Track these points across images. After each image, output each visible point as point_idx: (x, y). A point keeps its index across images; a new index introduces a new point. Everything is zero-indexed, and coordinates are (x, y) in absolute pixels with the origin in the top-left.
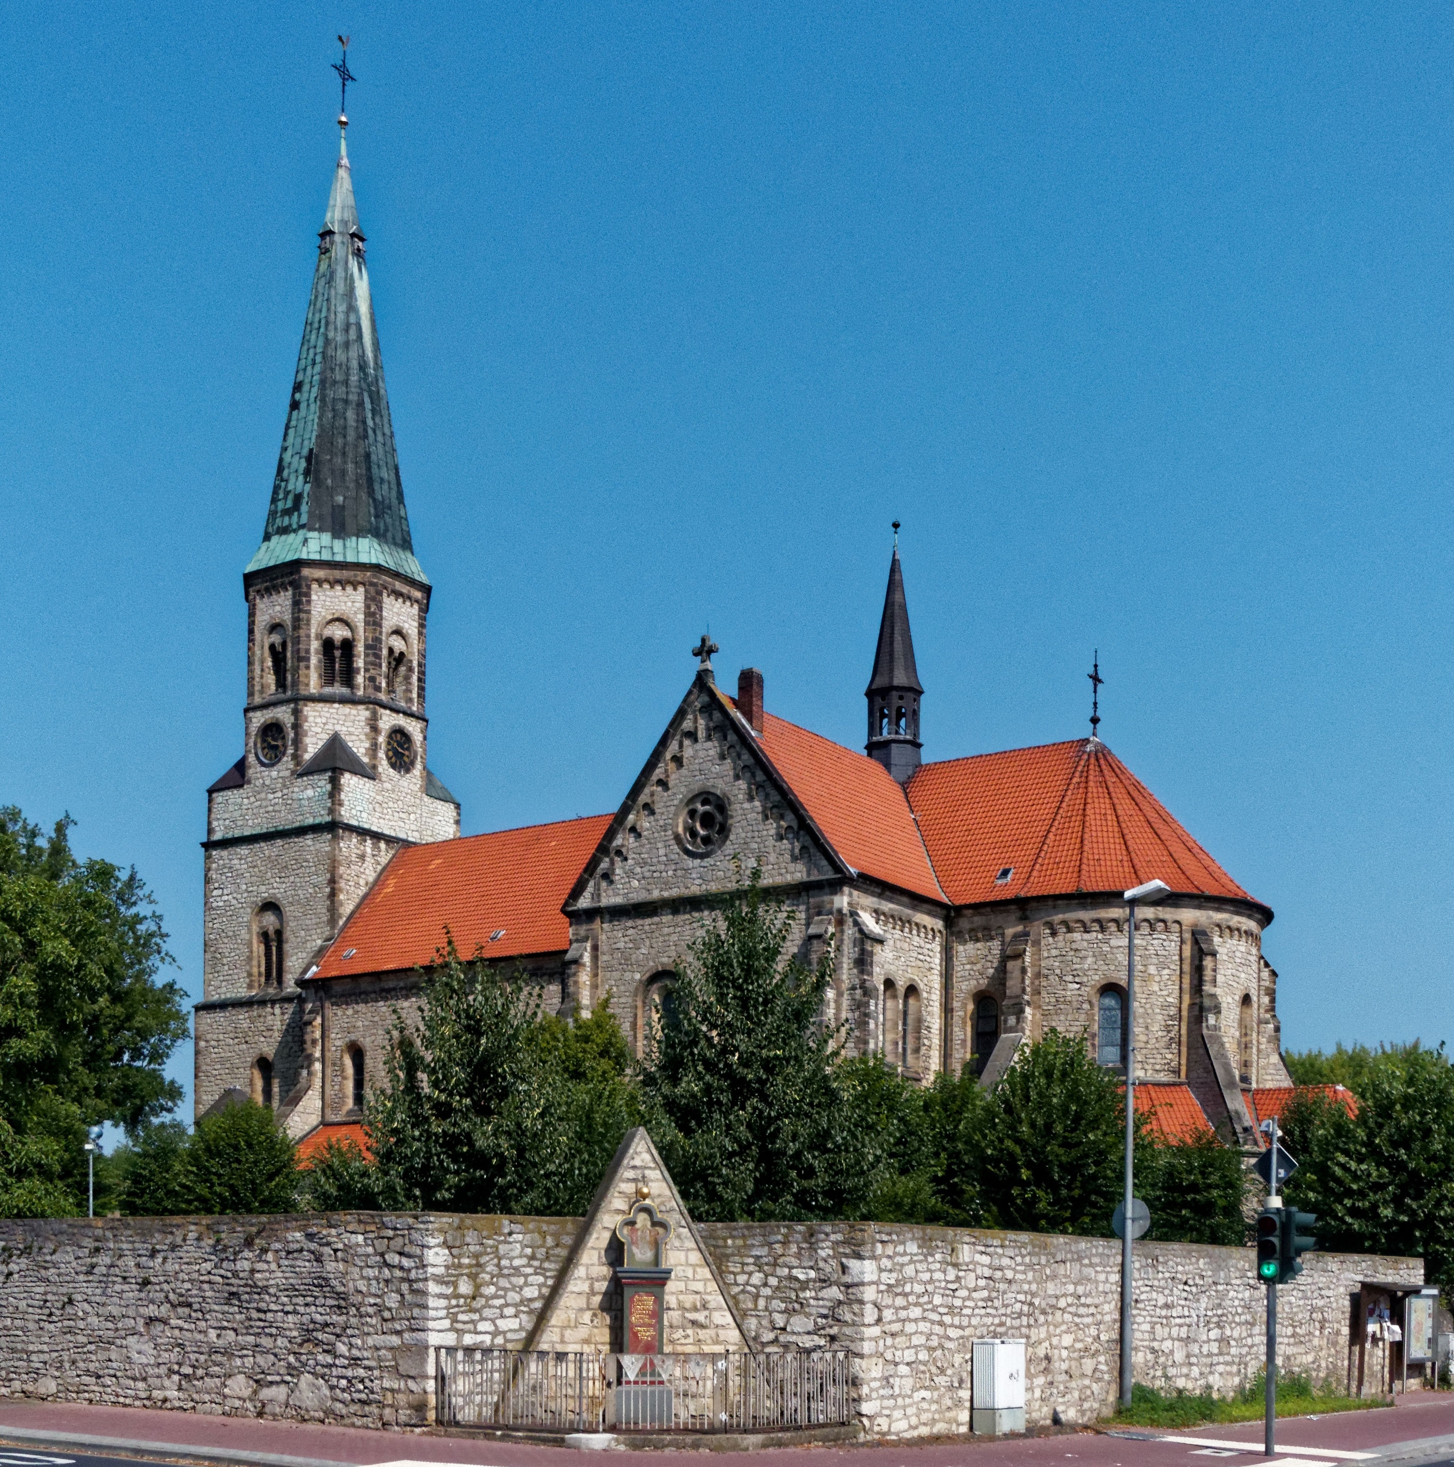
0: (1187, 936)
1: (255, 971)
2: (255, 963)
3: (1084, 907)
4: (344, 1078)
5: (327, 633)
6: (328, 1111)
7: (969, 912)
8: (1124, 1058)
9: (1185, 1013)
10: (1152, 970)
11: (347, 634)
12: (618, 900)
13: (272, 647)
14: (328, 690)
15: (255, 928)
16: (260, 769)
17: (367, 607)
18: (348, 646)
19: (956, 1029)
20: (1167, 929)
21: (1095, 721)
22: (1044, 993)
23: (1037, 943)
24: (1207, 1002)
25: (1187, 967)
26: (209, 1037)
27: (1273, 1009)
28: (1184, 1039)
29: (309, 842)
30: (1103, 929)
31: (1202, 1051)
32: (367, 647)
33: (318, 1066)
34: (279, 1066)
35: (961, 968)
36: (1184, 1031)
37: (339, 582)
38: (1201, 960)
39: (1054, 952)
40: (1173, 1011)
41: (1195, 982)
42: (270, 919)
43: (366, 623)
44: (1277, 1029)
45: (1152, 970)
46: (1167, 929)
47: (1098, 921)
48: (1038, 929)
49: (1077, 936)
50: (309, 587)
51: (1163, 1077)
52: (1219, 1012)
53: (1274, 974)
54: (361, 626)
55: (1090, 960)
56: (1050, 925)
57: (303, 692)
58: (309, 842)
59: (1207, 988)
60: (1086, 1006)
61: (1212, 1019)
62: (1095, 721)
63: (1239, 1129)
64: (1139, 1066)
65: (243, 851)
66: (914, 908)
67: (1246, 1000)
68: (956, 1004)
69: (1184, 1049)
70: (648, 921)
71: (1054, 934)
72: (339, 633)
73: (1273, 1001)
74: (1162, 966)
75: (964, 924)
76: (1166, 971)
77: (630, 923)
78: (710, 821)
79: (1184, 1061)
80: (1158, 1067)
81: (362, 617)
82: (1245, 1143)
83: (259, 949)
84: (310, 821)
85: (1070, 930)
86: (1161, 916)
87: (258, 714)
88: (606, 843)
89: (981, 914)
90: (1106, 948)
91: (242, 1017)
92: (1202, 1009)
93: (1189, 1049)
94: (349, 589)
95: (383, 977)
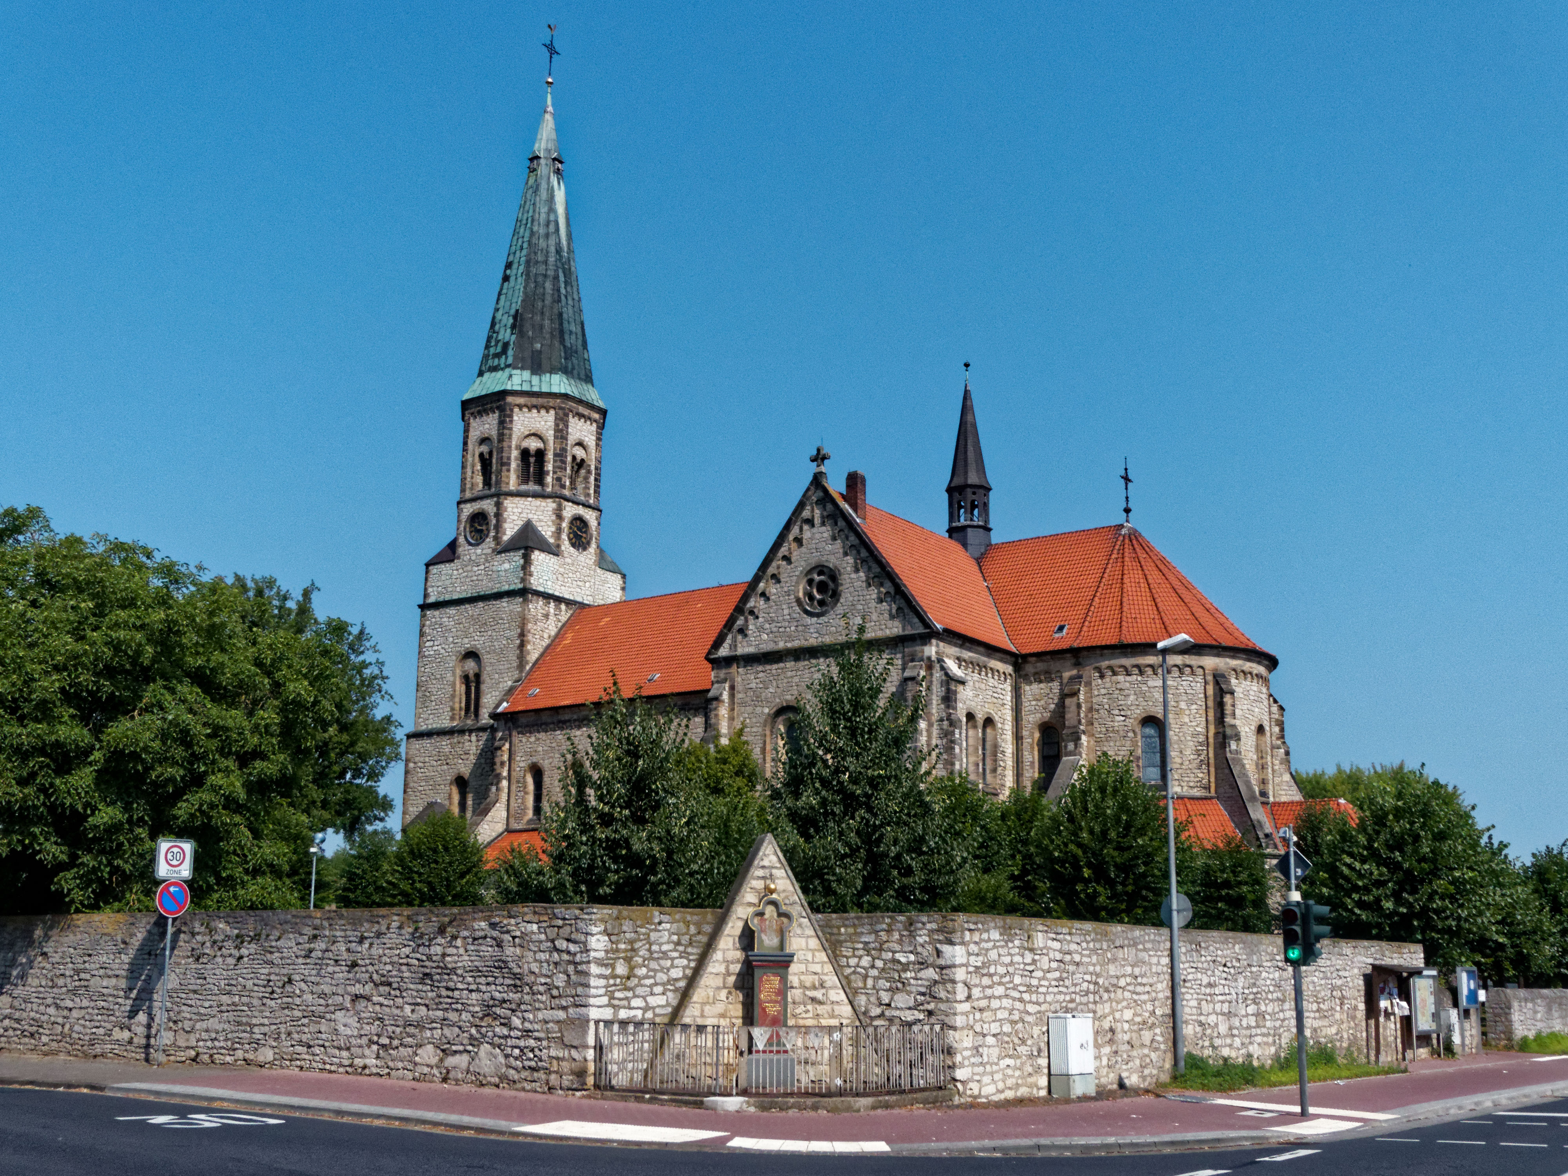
0: (1210, 678)
1: (457, 706)
2: (457, 700)
3: (1125, 655)
4: (526, 793)
5: (525, 444)
6: (512, 820)
7: (1033, 659)
8: (1164, 777)
9: (1211, 740)
10: (1183, 705)
11: (540, 445)
12: (751, 650)
13: (481, 455)
14: (524, 487)
15: (458, 672)
16: (467, 547)
17: (557, 425)
18: (540, 454)
19: (1025, 753)
20: (1193, 673)
21: (1127, 511)
22: (1096, 724)
23: (1088, 684)
24: (1229, 731)
25: (1211, 703)
26: (417, 759)
27: (1283, 737)
28: (1212, 761)
29: (505, 604)
30: (1141, 673)
31: (1227, 771)
32: (555, 455)
33: (505, 783)
34: (473, 784)
35: (1028, 704)
36: (1211, 755)
37: (535, 407)
38: (1222, 698)
39: (1103, 691)
40: (1202, 738)
41: (1219, 715)
42: (471, 666)
43: (556, 437)
44: (1287, 753)
45: (1183, 705)
46: (1193, 673)
47: (1137, 666)
48: (1088, 672)
49: (1121, 678)
50: (512, 410)
51: (1196, 792)
52: (1239, 739)
53: (1281, 708)
54: (551, 440)
55: (1132, 697)
56: (1099, 670)
57: (504, 489)
58: (505, 604)
59: (1228, 720)
60: (1131, 734)
61: (1233, 745)
62: (1127, 511)
63: (1261, 835)
64: (1177, 783)
65: (452, 611)
66: (989, 656)
67: (1260, 729)
68: (1025, 733)
69: (1212, 770)
70: (775, 666)
71: (1102, 676)
72: (534, 445)
73: (1282, 730)
74: (1191, 702)
75: (1029, 668)
76: (1194, 707)
77: (760, 668)
78: (825, 587)
79: (1213, 779)
80: (1192, 784)
81: (552, 432)
82: (1267, 847)
83: (461, 688)
84: (506, 588)
85: (1115, 673)
86: (1188, 663)
87: (468, 505)
88: (741, 606)
89: (1042, 661)
90: (1145, 688)
91: (445, 744)
92: (1225, 737)
93: (1216, 769)
94: (543, 412)
95: (561, 711)
